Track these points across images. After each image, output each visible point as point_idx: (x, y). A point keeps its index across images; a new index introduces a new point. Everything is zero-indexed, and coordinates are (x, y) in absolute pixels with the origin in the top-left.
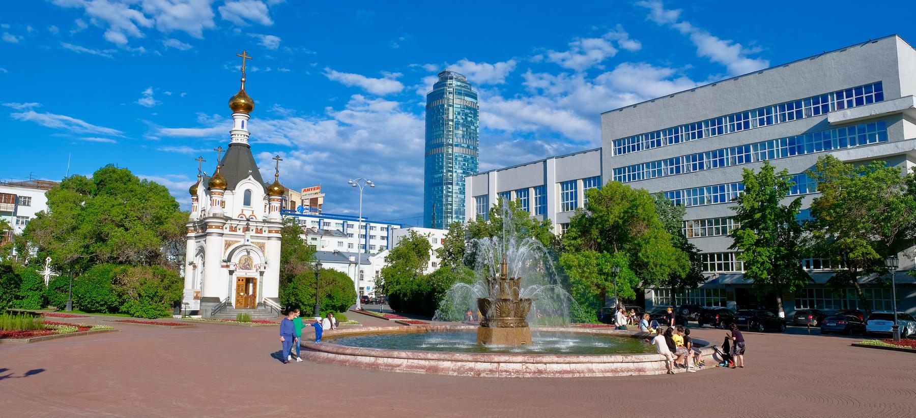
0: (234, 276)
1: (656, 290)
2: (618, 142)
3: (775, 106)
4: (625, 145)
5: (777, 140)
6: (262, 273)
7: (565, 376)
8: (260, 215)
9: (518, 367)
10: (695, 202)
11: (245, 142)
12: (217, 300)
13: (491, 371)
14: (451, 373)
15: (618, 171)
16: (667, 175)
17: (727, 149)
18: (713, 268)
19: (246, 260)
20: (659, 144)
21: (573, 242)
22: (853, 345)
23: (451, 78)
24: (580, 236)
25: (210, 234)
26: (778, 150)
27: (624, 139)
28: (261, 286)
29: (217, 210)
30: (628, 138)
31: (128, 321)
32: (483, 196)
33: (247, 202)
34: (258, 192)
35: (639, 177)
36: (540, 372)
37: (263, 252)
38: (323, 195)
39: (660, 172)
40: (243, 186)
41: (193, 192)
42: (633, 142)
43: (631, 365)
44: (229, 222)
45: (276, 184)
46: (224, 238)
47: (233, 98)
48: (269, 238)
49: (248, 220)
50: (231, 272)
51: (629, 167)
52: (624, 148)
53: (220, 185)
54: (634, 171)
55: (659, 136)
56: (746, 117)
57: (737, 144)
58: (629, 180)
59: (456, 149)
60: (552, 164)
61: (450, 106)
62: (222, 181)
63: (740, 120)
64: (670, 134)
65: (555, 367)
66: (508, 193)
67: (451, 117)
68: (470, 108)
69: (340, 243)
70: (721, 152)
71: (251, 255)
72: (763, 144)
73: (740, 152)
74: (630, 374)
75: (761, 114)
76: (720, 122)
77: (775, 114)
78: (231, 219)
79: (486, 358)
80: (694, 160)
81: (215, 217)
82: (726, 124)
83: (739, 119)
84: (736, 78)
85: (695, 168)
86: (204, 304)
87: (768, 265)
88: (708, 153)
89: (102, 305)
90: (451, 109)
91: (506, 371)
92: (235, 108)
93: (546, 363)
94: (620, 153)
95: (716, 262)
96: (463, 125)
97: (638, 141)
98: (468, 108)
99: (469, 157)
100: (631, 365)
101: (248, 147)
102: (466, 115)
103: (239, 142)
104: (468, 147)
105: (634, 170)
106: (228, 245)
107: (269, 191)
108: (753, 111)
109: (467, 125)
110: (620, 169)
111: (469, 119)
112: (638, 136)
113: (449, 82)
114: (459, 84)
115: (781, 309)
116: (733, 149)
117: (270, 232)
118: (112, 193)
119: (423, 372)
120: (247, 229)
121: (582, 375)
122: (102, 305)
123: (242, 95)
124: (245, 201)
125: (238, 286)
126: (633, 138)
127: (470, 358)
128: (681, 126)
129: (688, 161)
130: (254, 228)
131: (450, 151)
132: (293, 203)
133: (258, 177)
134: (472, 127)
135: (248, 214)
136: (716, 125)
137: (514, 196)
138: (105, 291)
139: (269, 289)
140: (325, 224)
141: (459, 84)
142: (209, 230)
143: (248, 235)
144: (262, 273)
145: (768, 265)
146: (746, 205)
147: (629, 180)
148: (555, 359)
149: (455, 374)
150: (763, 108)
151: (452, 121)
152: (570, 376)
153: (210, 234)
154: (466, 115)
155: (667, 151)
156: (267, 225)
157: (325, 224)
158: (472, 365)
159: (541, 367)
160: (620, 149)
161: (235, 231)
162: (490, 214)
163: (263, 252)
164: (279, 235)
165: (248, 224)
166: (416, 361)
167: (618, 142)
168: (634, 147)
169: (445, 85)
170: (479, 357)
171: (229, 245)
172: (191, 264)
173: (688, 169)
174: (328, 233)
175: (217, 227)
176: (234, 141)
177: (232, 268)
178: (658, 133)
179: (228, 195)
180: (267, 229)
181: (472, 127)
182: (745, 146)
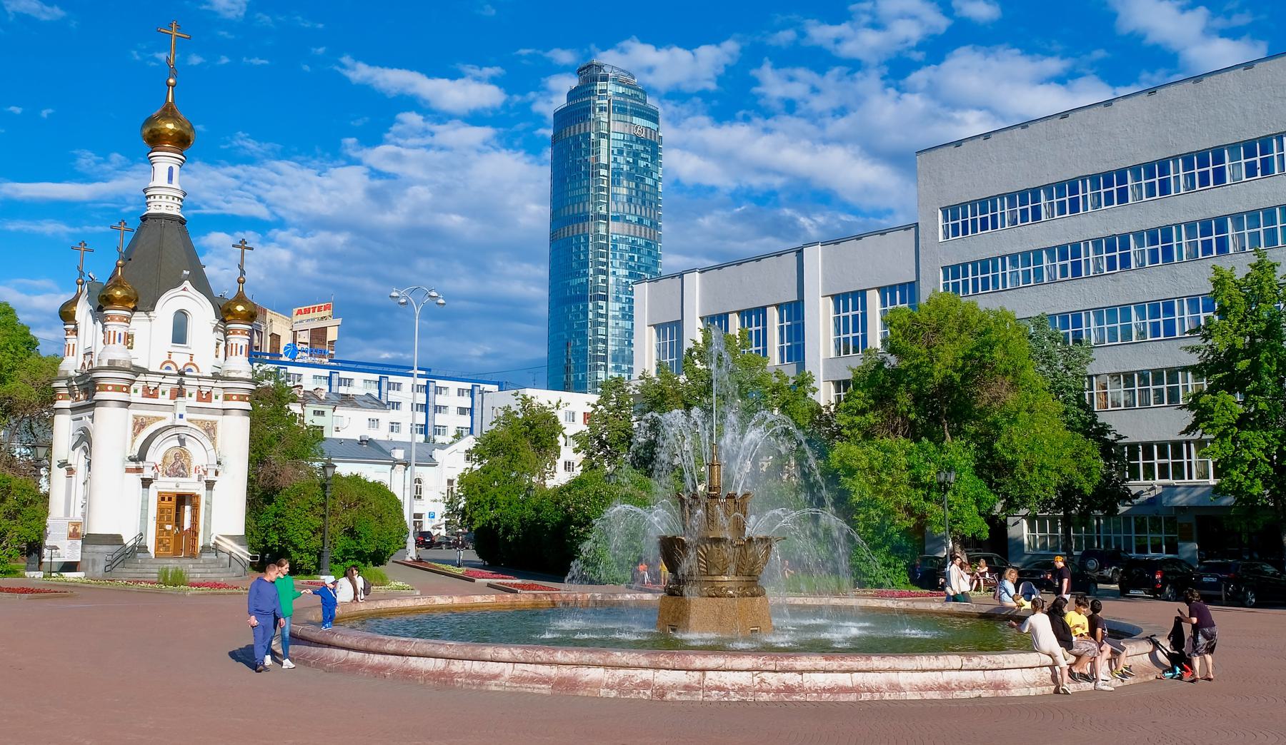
1: (1031, 520)
2: (951, 212)
4: (968, 217)
6: (210, 485)
7: (842, 698)
9: (744, 679)
11: (175, 211)
12: (116, 539)
13: (688, 688)
14: (603, 692)
15: (953, 271)
16: (1053, 281)
17: (1178, 226)
21: (857, 419)
23: (605, 79)
24: (873, 408)
27: (964, 205)
30: (973, 203)
32: (671, 324)
33: (180, 336)
34: (202, 314)
36: (789, 689)
37: (213, 439)
38: (339, 321)
39: (1038, 273)
40: (169, 304)
42: (984, 211)
43: (979, 677)
44: (142, 377)
45: (240, 298)
46: (132, 412)
47: (150, 121)
48: (225, 411)
49: (182, 374)
50: (146, 483)
51: (974, 264)
53: (124, 301)
55: (1036, 199)
56: (1219, 158)
58: (975, 289)
60: (815, 257)
61: (602, 136)
62: (126, 292)
64: (1061, 193)
66: (723, 318)
67: (603, 160)
68: (642, 141)
70: (1167, 232)
71: (189, 446)
72: (1253, 216)
74: (976, 693)
75: (1250, 152)
76: (1164, 170)
78: (146, 372)
80: (1111, 248)
81: (112, 367)
82: (1177, 174)
84: (1197, 79)
85: (1111, 265)
86: (89, 548)
87: (1264, 468)
88: (1139, 236)
90: (604, 142)
92: (155, 140)
93: (801, 672)
94: (956, 233)
95: (1157, 461)
96: (630, 177)
98: (639, 140)
100: (979, 677)
102: (636, 155)
103: (163, 210)
104: (640, 221)
105: (985, 270)
106: (139, 425)
107: (225, 313)
108: (1233, 147)
111: (642, 164)
112: (993, 199)
113: (600, 86)
114: (621, 90)
116: (1190, 226)
117: (227, 398)
119: (545, 689)
121: (877, 696)
123: (169, 112)
124: (174, 335)
125: (161, 511)
127: (644, 661)
128: (1083, 179)
129: (1097, 249)
130: (195, 391)
133: (202, 285)
134: (649, 181)
135: (181, 360)
137: (735, 323)
139: (226, 517)
141: (621, 90)
143: (182, 404)
144: (210, 485)
145: (1264, 468)
148: (820, 662)
149: (613, 694)
152: (852, 697)
153: (102, 402)
154: (636, 155)
156: (220, 384)
157: (343, 382)
158: (648, 675)
160: (955, 227)
161: (155, 396)
162: (685, 362)
163: (213, 439)
164: (247, 406)
165: (181, 383)
167: (951, 212)
168: (984, 221)
169: (592, 93)
170: (662, 659)
171: (143, 426)
173: (1097, 268)
174: (347, 400)
176: (152, 210)
177: (148, 473)
179: (139, 323)
180: (221, 393)
181: (649, 181)
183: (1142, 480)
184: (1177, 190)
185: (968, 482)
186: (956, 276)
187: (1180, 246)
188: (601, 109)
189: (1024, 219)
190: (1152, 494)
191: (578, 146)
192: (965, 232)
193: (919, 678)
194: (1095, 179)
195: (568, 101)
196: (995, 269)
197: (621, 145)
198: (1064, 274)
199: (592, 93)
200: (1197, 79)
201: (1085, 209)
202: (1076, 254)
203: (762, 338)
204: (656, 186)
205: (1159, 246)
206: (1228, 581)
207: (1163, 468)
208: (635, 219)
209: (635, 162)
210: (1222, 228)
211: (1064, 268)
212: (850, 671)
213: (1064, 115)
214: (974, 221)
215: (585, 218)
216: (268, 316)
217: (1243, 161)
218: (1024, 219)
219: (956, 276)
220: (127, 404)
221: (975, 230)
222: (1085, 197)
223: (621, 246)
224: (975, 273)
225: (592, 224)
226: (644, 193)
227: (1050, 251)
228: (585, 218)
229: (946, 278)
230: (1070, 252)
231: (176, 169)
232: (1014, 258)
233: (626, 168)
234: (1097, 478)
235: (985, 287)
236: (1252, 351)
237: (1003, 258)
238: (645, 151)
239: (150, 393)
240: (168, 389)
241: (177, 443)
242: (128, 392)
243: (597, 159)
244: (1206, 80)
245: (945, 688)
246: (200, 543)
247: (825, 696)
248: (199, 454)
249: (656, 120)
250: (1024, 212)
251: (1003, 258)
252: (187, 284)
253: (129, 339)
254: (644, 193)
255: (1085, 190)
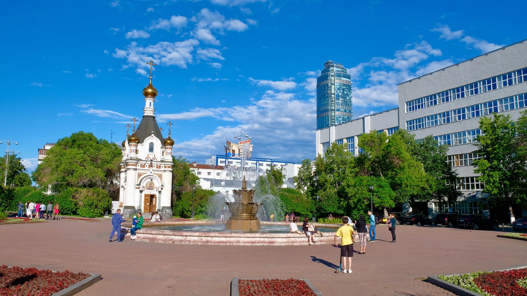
0: (143, 194)
1: (435, 203)
2: (409, 103)
3: (514, 72)
4: (415, 104)
5: (516, 96)
6: (160, 192)
7: (221, 244)
8: (159, 158)
9: (196, 239)
10: (460, 142)
11: (152, 115)
12: (133, 207)
13: (181, 241)
14: (160, 242)
15: (410, 122)
16: (441, 124)
17: (481, 104)
18: (473, 187)
19: (150, 184)
20: (435, 103)
21: (353, 170)
22: (498, 236)
23: (333, 66)
24: (358, 166)
25: (129, 169)
26: (517, 103)
27: (413, 101)
28: (160, 200)
29: (133, 155)
30: (415, 100)
31: (82, 219)
32: (327, 143)
33: (151, 149)
34: (157, 143)
35: (423, 126)
36: (208, 242)
37: (161, 179)
38: (252, 145)
39: (436, 122)
40: (148, 141)
41: (123, 145)
42: (419, 102)
43: (266, 240)
44: (140, 162)
45: (169, 139)
46: (137, 171)
47: (145, 89)
48: (165, 171)
49: (152, 161)
50: (141, 192)
51: (416, 120)
52: (413, 107)
53: (134, 140)
54: (419, 123)
55: (435, 98)
56: (494, 81)
57: (489, 100)
58: (417, 128)
59: (337, 113)
60: (368, 120)
61: (332, 84)
62: (137, 138)
63: (490, 83)
64: (443, 95)
65: (217, 239)
66: (342, 140)
67: (333, 92)
68: (346, 85)
69: (209, 173)
70: (477, 106)
71: (153, 181)
72: (506, 99)
73: (490, 105)
74: (262, 244)
75: (505, 78)
76: (476, 86)
77: (515, 77)
78: (141, 160)
79: (179, 233)
80: (459, 112)
81: (131, 159)
82: (481, 86)
83: (489, 82)
84: (486, 54)
85: (459, 118)
86: (125, 210)
87: (497, 184)
88: (468, 108)
89: (68, 210)
90: (333, 86)
91: (189, 241)
92: (146, 94)
93: (212, 237)
94: (410, 110)
95: (475, 183)
96: (342, 97)
97: (422, 102)
98: (344, 85)
99: (346, 117)
100: (266, 240)
101: (154, 117)
102: (343, 90)
103: (148, 114)
104: (345, 111)
105: (420, 122)
106: (140, 175)
107: (164, 143)
108: (499, 77)
109: (344, 96)
110: (410, 121)
111: (345, 92)
112: (422, 98)
113: (331, 68)
114: (338, 69)
115: (512, 215)
116: (485, 104)
117: (165, 167)
118: (79, 147)
119: (147, 241)
120: (151, 166)
121: (231, 244)
122: (68, 210)
123: (150, 86)
124: (150, 150)
125: (145, 199)
126: (419, 100)
127: (171, 233)
128: (450, 90)
129: (455, 113)
130: (156, 165)
131: (333, 114)
132: (234, 151)
133: (159, 135)
134: (348, 98)
135: (151, 157)
136: (474, 87)
137: (345, 141)
138: (68, 202)
139: (165, 200)
140: (260, 165)
141: (338, 69)
142: (128, 167)
143: (151, 169)
144: (160, 192)
145: (497, 184)
146: (482, 142)
147: (417, 128)
148: (217, 234)
149: (162, 242)
150: (506, 74)
151: (334, 94)
152: (224, 244)
153: (129, 169)
154: (343, 90)
155: (441, 107)
156: (163, 163)
157: (260, 165)
158: (173, 237)
159: (209, 239)
160: (410, 108)
161: (144, 167)
162: (362, 156)
163: (161, 179)
164: (171, 169)
165: (151, 163)
166: (147, 235)
167: (409, 103)
168: (419, 106)
169: (329, 71)
170: (176, 233)
171: (141, 175)
172: (123, 187)
173: (455, 119)
174: (246, 169)
175: (132, 165)
176: (145, 114)
177: (141, 189)
178: (435, 95)
179: (140, 146)
180: (163, 166)
181: (348, 98)
182: (494, 101)
183: (470, 189)
184: (481, 92)
185: (388, 189)
186: (411, 124)
187: (482, 111)
188: (332, 76)
189: (432, 104)
190: (474, 194)
191: (325, 88)
192: (413, 110)
193: (246, 240)
194: (453, 90)
195: (322, 73)
196: (423, 121)
197: (339, 87)
198: (444, 122)
199: (329, 71)
200: (486, 54)
201: (451, 100)
202: (448, 115)
203: (353, 146)
204: (350, 99)
205: (475, 111)
206: (468, 221)
207: (477, 185)
208: (343, 110)
209: (343, 92)
210: (496, 104)
211: (444, 120)
212: (226, 237)
213: (443, 69)
214: (416, 106)
215: (327, 111)
216: (232, 145)
217: (502, 81)
218: (432, 104)
219: (411, 124)
220: (136, 169)
221: (416, 109)
222: (451, 96)
223: (339, 119)
224: (416, 123)
225: (330, 113)
226: (346, 102)
227: (440, 114)
228: (327, 111)
229: (408, 125)
230: (446, 115)
231: (152, 103)
232: (428, 117)
233: (340, 94)
234: (434, 188)
235: (420, 127)
236: (493, 144)
237: (425, 117)
238: (347, 88)
239: (143, 166)
240: (148, 165)
241: (150, 180)
242: (136, 166)
243: (331, 92)
244: (489, 54)
245: (253, 242)
246: (157, 209)
247: (216, 244)
248: (157, 183)
249: (350, 78)
250: (431, 102)
251: (425, 117)
252: (153, 135)
253: (137, 151)
254: (346, 102)
255: (450, 94)
